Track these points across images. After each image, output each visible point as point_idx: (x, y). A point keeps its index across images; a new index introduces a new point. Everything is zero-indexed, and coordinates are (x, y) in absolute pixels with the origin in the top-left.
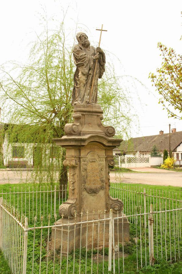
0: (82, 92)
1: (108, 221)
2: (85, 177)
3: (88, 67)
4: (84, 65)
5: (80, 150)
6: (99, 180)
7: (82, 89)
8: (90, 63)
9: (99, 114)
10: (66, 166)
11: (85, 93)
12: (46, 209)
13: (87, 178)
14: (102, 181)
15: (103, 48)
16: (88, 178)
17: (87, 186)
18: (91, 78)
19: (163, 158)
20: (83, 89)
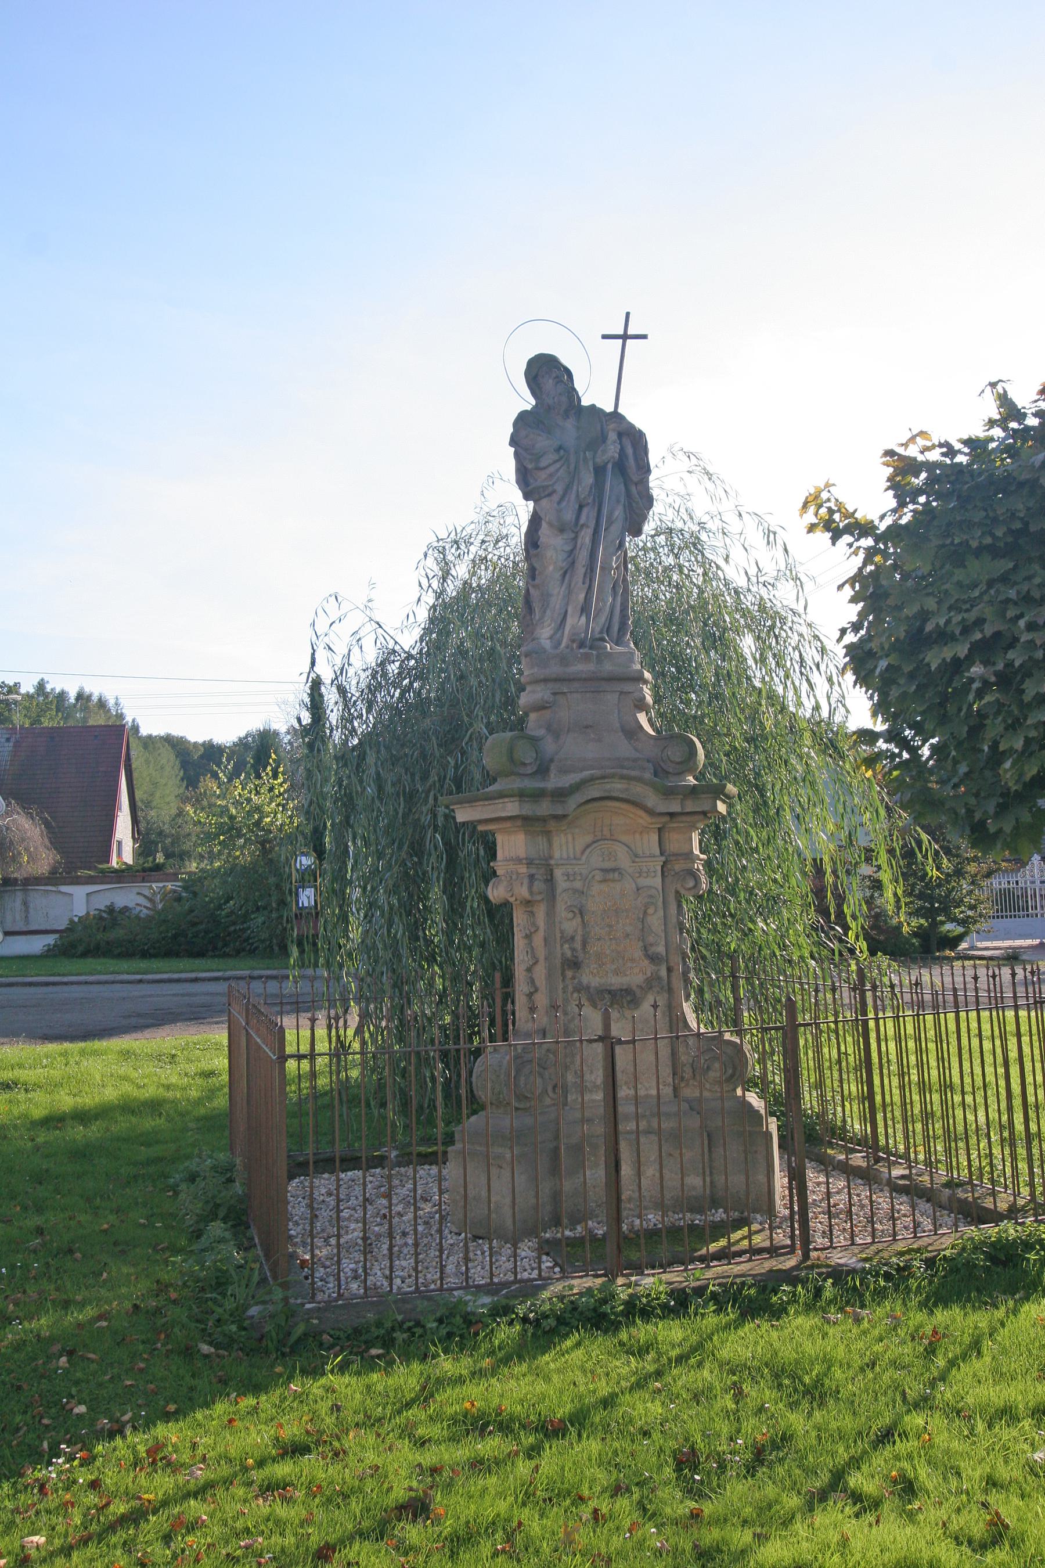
0: (556, 602)
1: (458, 1051)
2: (578, 945)
3: (573, 496)
4: (554, 491)
5: (548, 834)
6: (638, 954)
7: (555, 592)
8: (579, 483)
9: (628, 687)
10: (262, 745)
11: (567, 604)
12: (927, 1116)
13: (584, 944)
14: (654, 959)
15: (634, 414)
16: (593, 948)
17: (590, 977)
18: (588, 540)
19: (982, 435)
20: (557, 591)
